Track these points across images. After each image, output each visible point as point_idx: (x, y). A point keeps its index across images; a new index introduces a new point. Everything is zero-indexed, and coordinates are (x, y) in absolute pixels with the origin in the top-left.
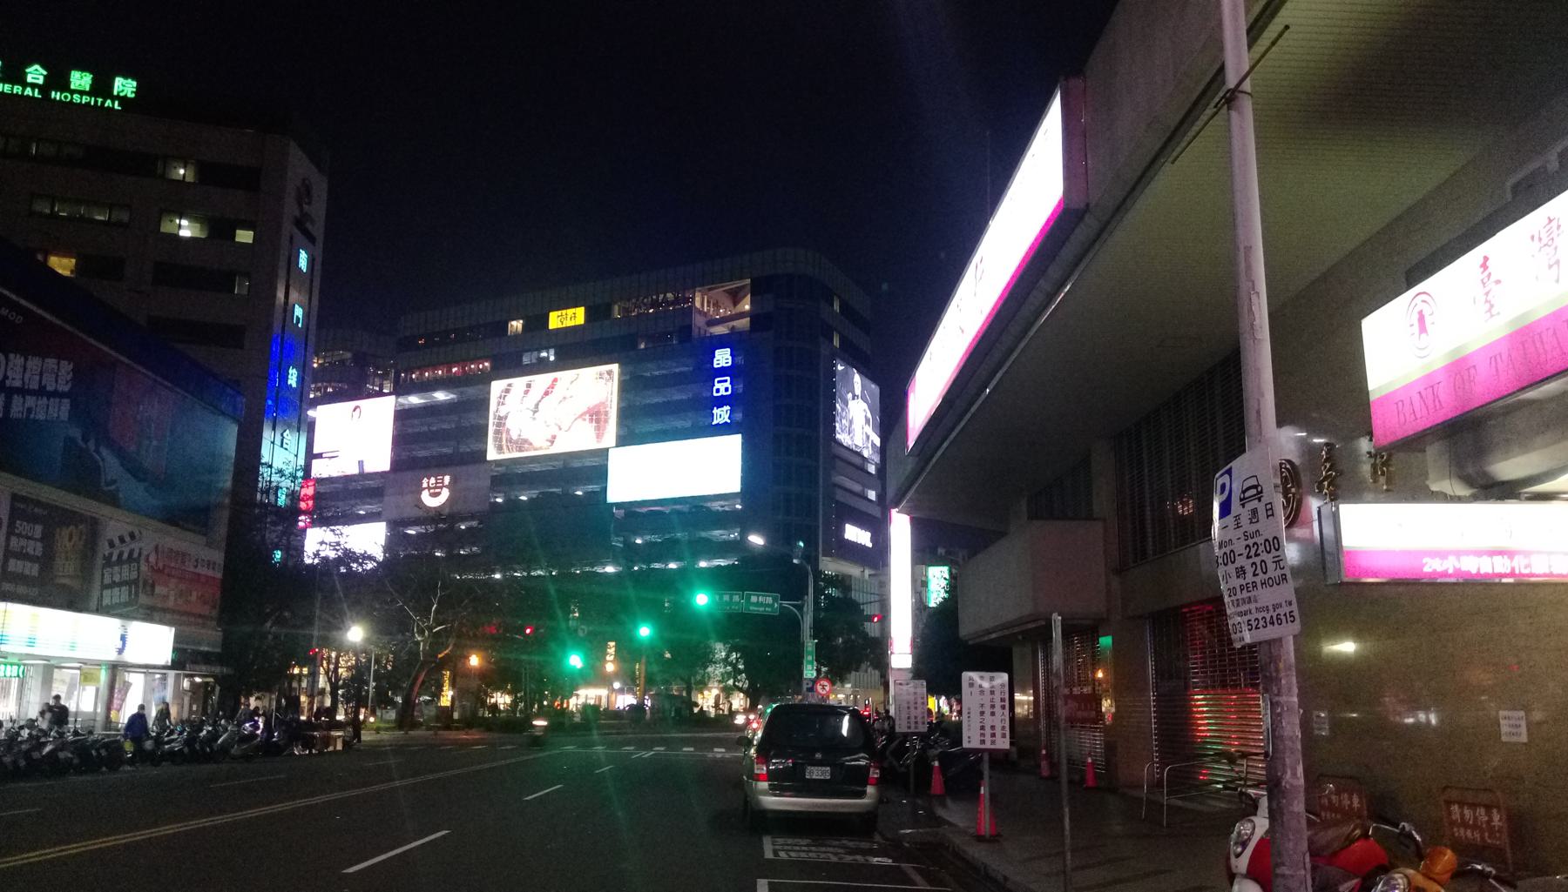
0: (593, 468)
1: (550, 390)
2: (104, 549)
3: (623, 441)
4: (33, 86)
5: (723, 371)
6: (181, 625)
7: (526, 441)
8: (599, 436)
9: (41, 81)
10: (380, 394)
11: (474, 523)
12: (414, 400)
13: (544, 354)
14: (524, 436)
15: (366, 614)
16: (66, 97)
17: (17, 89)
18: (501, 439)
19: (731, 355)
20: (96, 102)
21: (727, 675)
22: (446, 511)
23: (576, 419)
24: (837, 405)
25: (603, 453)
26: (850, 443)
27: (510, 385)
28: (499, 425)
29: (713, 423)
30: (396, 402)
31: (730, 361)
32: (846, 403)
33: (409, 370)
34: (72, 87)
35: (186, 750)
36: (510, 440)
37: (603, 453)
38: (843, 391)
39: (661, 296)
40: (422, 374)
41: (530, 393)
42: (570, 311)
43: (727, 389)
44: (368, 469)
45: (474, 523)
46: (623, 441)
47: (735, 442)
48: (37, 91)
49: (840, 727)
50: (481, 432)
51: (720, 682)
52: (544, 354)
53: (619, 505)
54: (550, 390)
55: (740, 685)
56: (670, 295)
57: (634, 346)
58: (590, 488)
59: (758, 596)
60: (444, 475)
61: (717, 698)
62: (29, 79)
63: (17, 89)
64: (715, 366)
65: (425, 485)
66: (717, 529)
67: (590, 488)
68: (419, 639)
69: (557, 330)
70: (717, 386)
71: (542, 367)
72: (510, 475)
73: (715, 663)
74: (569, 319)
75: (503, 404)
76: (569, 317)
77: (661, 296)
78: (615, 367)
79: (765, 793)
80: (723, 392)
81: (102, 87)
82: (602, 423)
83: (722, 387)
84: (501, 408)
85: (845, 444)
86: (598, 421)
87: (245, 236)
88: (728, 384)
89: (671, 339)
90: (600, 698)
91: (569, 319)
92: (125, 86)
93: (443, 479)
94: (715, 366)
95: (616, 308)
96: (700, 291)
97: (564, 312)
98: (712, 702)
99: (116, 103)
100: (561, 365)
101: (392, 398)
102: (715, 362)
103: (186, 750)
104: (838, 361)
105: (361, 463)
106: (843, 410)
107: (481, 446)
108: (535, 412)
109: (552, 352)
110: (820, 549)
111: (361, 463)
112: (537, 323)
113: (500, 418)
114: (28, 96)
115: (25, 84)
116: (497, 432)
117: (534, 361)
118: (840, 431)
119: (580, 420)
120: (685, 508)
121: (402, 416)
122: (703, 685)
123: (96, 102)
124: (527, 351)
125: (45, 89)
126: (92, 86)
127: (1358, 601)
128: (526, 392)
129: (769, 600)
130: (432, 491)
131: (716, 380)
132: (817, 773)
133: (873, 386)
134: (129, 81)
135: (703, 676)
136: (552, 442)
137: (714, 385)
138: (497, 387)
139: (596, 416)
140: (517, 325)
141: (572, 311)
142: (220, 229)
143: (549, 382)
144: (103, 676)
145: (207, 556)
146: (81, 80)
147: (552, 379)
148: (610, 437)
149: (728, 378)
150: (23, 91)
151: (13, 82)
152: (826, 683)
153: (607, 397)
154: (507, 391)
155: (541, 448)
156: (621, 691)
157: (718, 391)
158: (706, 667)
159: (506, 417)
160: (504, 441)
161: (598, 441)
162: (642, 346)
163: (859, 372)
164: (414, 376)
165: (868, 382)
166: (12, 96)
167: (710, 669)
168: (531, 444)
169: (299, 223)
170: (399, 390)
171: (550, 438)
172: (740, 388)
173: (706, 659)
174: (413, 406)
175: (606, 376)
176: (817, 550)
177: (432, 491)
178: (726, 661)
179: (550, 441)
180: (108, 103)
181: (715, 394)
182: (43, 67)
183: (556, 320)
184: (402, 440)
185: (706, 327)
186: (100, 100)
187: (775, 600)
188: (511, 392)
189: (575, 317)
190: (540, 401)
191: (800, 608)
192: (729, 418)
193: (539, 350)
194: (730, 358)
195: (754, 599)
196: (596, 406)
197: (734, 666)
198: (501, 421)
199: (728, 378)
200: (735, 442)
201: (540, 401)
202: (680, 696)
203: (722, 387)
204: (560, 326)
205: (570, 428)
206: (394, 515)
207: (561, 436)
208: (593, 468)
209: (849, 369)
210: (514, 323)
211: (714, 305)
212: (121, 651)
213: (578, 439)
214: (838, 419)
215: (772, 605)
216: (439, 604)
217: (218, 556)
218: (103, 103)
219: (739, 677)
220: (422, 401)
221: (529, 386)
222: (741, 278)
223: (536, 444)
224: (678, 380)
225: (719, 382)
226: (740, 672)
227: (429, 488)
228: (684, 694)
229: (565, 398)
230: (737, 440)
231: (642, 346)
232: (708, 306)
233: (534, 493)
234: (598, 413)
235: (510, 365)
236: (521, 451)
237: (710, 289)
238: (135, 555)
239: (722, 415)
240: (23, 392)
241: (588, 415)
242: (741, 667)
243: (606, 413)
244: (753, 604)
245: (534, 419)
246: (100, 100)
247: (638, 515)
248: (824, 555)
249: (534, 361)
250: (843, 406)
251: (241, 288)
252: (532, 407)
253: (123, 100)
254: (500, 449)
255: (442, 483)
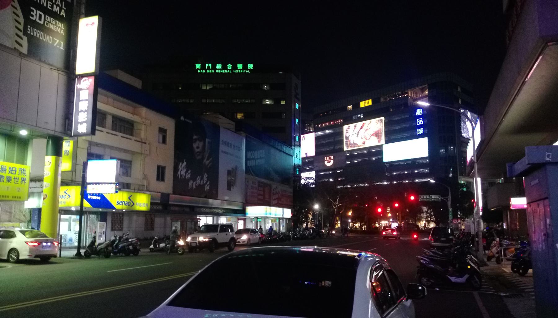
0: (378, 151)
1: (362, 127)
2: (273, 191)
3: (387, 142)
4: (229, 70)
5: (420, 117)
6: (318, 215)
7: (356, 144)
8: (379, 141)
9: (231, 68)
10: (310, 132)
11: (342, 170)
12: (320, 133)
13: (359, 116)
14: (355, 142)
15: (319, 201)
16: (237, 71)
17: (226, 71)
18: (348, 144)
19: (422, 111)
20: (244, 71)
21: (427, 217)
22: (333, 167)
23: (371, 136)
24: (462, 124)
25: (381, 146)
26: (467, 136)
27: (349, 127)
28: (347, 139)
29: (418, 134)
30: (315, 134)
31: (422, 113)
32: (465, 123)
33: (318, 125)
34: (238, 68)
35: (300, 237)
36: (350, 144)
37: (381, 146)
38: (464, 118)
39: (397, 93)
40: (322, 125)
41: (356, 128)
42: (367, 101)
43: (421, 122)
44: (309, 155)
45: (342, 170)
46: (387, 142)
47: (425, 140)
48: (230, 71)
49: (230, 229)
50: (341, 142)
51: (425, 219)
52: (359, 116)
53: (387, 163)
54: (362, 127)
55: (432, 220)
56: (400, 92)
57: (389, 110)
58: (377, 157)
59: (434, 196)
60: (331, 156)
61: (425, 224)
62: (228, 68)
63: (226, 71)
64: (417, 115)
65: (326, 159)
66: (421, 169)
67: (377, 157)
68: (334, 208)
69: (363, 108)
70: (418, 121)
71: (359, 120)
72: (352, 155)
73: (423, 213)
74: (367, 104)
75: (348, 133)
76: (367, 103)
77: (397, 93)
78: (383, 118)
79: (433, 243)
80: (420, 124)
81: (245, 67)
82: (380, 137)
83: (420, 122)
84: (347, 134)
85: (465, 137)
86: (378, 136)
87: (283, 103)
88: (422, 121)
89: (401, 107)
90: (387, 224)
91: (367, 104)
92: (250, 66)
93: (331, 157)
94: (417, 115)
95: (382, 99)
96: (410, 90)
97: (365, 101)
98: (423, 225)
99: (249, 71)
100: (365, 119)
101: (314, 133)
102: (417, 114)
103: (300, 237)
104: (461, 108)
105: (306, 154)
106: (464, 125)
107: (341, 146)
108: (358, 135)
109: (362, 115)
110: (458, 174)
111: (306, 154)
112: (356, 106)
113: (347, 137)
114: (228, 73)
115: (227, 70)
116: (346, 142)
117: (356, 118)
118: (463, 133)
119: (373, 136)
120: (410, 162)
121: (317, 139)
122: (420, 220)
123: (244, 71)
124: (354, 115)
125: (232, 70)
126: (243, 67)
127: (464, 225)
128: (355, 128)
129: (438, 197)
130: (328, 161)
131: (418, 120)
132: (443, 239)
133: (475, 115)
134: (251, 64)
135: (420, 217)
136: (364, 144)
137: (417, 121)
138: (345, 127)
139: (377, 134)
140: (350, 107)
141: (368, 101)
142: (277, 101)
143: (362, 125)
144: (277, 221)
145: (289, 190)
146: (240, 66)
147: (362, 124)
148: (383, 141)
149: (422, 119)
150: (227, 71)
151: (225, 70)
152: (455, 220)
153: (381, 128)
154: (349, 128)
155: (361, 146)
156: (393, 222)
157: (418, 123)
158: (421, 214)
159: (349, 137)
160: (349, 144)
161: (379, 143)
162: (391, 110)
163: (470, 111)
164: (319, 126)
165: (473, 114)
166: (225, 73)
167: (422, 215)
168: (357, 145)
169: (296, 96)
170: (315, 131)
171: (363, 142)
172: (426, 121)
173: (421, 211)
174: (320, 135)
175: (380, 121)
176: (457, 174)
177: (328, 161)
178: (427, 212)
179: (363, 144)
180: (247, 71)
181: (417, 124)
182: (231, 64)
183: (362, 105)
184: (317, 146)
185: (412, 102)
186: (245, 71)
187: (439, 197)
188: (350, 129)
189: (369, 102)
190: (359, 131)
191: (447, 199)
192: (423, 132)
193: (358, 114)
194: (422, 112)
195: (433, 197)
196: (377, 131)
197: (430, 214)
198: (347, 138)
199: (422, 119)
200: (425, 140)
201: (359, 131)
202: (412, 224)
203: (420, 122)
204: (364, 106)
205: (369, 139)
206: (317, 169)
207: (367, 142)
208: (378, 151)
209: (466, 111)
210: (349, 106)
211: (415, 93)
212: (283, 215)
213: (373, 142)
214: (462, 129)
215: (438, 199)
216: (339, 198)
217: (291, 190)
218: (246, 71)
219: (432, 217)
220: (323, 133)
221: (355, 126)
222: (424, 85)
223: (359, 145)
224: (404, 121)
225: (418, 120)
226: (432, 216)
227: (327, 160)
228: (414, 223)
229: (367, 129)
230: (426, 139)
231: (391, 110)
232: (413, 94)
233: (359, 160)
234: (378, 133)
235: (349, 120)
236: (354, 147)
237: (413, 89)
238: (278, 192)
239: (420, 131)
240: (258, 159)
241: (375, 135)
242: (432, 214)
243: (381, 133)
244: (433, 199)
245: (358, 137)
246: (245, 71)
247: (394, 166)
248: (460, 176)
249: (356, 118)
250: (464, 124)
251: (284, 116)
252: (357, 133)
253: (250, 70)
254: (348, 147)
255: (331, 158)
